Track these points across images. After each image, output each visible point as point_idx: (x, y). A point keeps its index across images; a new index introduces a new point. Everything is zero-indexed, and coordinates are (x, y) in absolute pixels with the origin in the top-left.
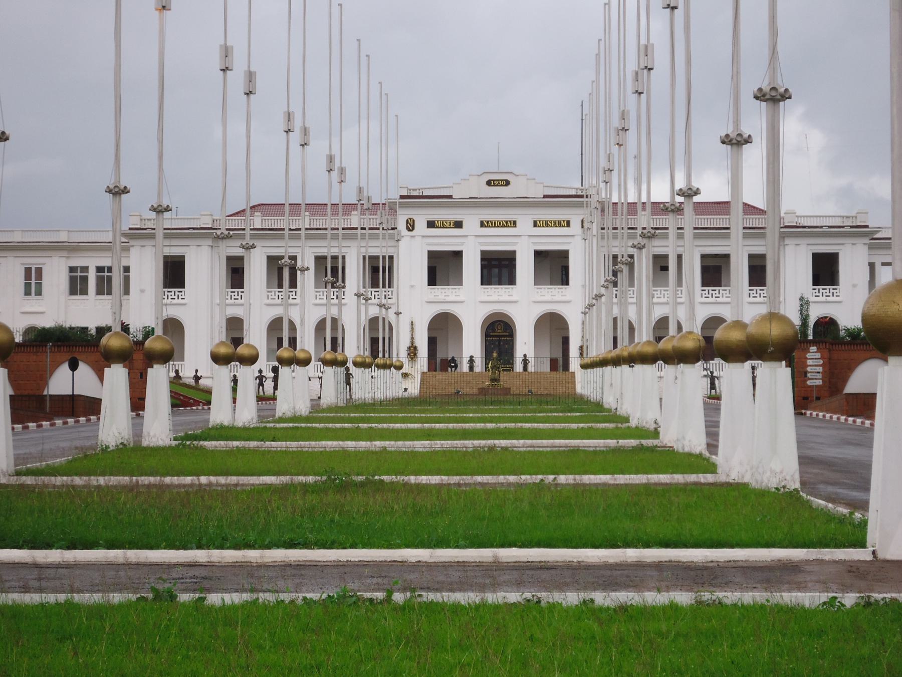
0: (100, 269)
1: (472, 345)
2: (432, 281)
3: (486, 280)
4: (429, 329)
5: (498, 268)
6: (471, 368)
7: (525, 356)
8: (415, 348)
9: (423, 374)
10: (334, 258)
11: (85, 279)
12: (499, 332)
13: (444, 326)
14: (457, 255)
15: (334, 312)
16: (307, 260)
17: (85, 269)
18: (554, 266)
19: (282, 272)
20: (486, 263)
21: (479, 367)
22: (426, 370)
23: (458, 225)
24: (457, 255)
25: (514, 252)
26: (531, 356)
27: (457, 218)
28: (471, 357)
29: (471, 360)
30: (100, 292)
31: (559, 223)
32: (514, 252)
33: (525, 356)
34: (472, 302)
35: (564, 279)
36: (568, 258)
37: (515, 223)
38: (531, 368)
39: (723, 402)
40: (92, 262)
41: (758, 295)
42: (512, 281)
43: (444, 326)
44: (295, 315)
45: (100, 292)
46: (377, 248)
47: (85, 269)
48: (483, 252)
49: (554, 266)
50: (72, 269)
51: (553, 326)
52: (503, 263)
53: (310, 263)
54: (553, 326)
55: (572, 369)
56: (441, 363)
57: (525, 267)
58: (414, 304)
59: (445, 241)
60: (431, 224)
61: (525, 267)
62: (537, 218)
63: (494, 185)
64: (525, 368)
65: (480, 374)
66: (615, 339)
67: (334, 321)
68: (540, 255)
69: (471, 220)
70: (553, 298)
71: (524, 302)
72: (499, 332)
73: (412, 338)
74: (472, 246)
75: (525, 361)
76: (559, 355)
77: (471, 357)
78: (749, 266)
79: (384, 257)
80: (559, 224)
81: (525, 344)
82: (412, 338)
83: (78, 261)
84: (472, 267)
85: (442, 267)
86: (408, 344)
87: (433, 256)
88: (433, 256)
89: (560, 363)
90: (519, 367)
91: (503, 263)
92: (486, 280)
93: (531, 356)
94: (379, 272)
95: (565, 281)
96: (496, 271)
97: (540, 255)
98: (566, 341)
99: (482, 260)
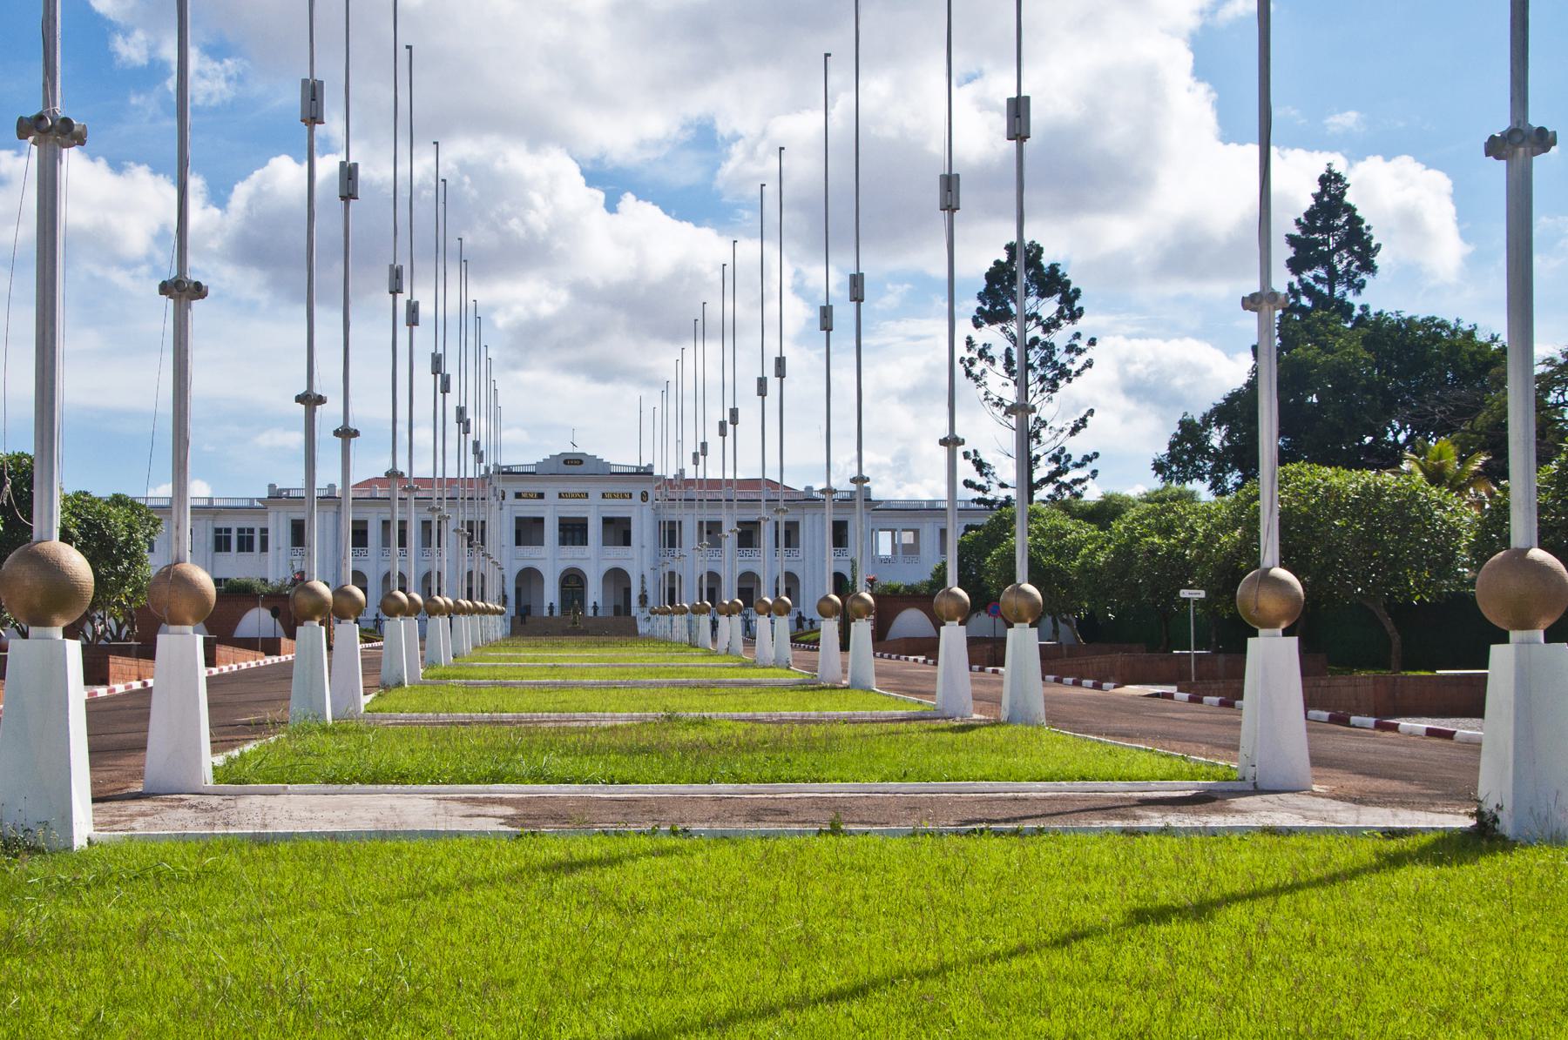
0: (240, 530)
1: (551, 594)
2: (518, 543)
3: (563, 541)
4: (517, 581)
5: (573, 531)
11: (228, 539)
12: (573, 582)
13: (529, 578)
14: (541, 520)
17: (228, 530)
18: (619, 531)
19: (748, 536)
21: (557, 613)
23: (541, 496)
24: (541, 520)
26: (557, 604)
30: (240, 549)
34: (551, 559)
35: (626, 541)
38: (600, 614)
40: (234, 524)
42: (541, 543)
43: (529, 578)
45: (240, 549)
46: (476, 515)
47: (228, 530)
49: (619, 531)
50: (218, 530)
51: (617, 578)
54: (617, 578)
57: (595, 530)
58: (504, 557)
59: (529, 509)
60: (518, 495)
61: (595, 530)
68: (607, 521)
69: (551, 491)
70: (616, 556)
71: (594, 559)
74: (551, 512)
75: (595, 608)
80: (623, 496)
81: (594, 593)
83: (222, 524)
84: (551, 531)
85: (528, 531)
87: (520, 521)
88: (520, 521)
89: (623, 609)
92: (563, 541)
93: (600, 604)
94: (475, 534)
96: (569, 535)
97: (607, 521)
98: (628, 591)
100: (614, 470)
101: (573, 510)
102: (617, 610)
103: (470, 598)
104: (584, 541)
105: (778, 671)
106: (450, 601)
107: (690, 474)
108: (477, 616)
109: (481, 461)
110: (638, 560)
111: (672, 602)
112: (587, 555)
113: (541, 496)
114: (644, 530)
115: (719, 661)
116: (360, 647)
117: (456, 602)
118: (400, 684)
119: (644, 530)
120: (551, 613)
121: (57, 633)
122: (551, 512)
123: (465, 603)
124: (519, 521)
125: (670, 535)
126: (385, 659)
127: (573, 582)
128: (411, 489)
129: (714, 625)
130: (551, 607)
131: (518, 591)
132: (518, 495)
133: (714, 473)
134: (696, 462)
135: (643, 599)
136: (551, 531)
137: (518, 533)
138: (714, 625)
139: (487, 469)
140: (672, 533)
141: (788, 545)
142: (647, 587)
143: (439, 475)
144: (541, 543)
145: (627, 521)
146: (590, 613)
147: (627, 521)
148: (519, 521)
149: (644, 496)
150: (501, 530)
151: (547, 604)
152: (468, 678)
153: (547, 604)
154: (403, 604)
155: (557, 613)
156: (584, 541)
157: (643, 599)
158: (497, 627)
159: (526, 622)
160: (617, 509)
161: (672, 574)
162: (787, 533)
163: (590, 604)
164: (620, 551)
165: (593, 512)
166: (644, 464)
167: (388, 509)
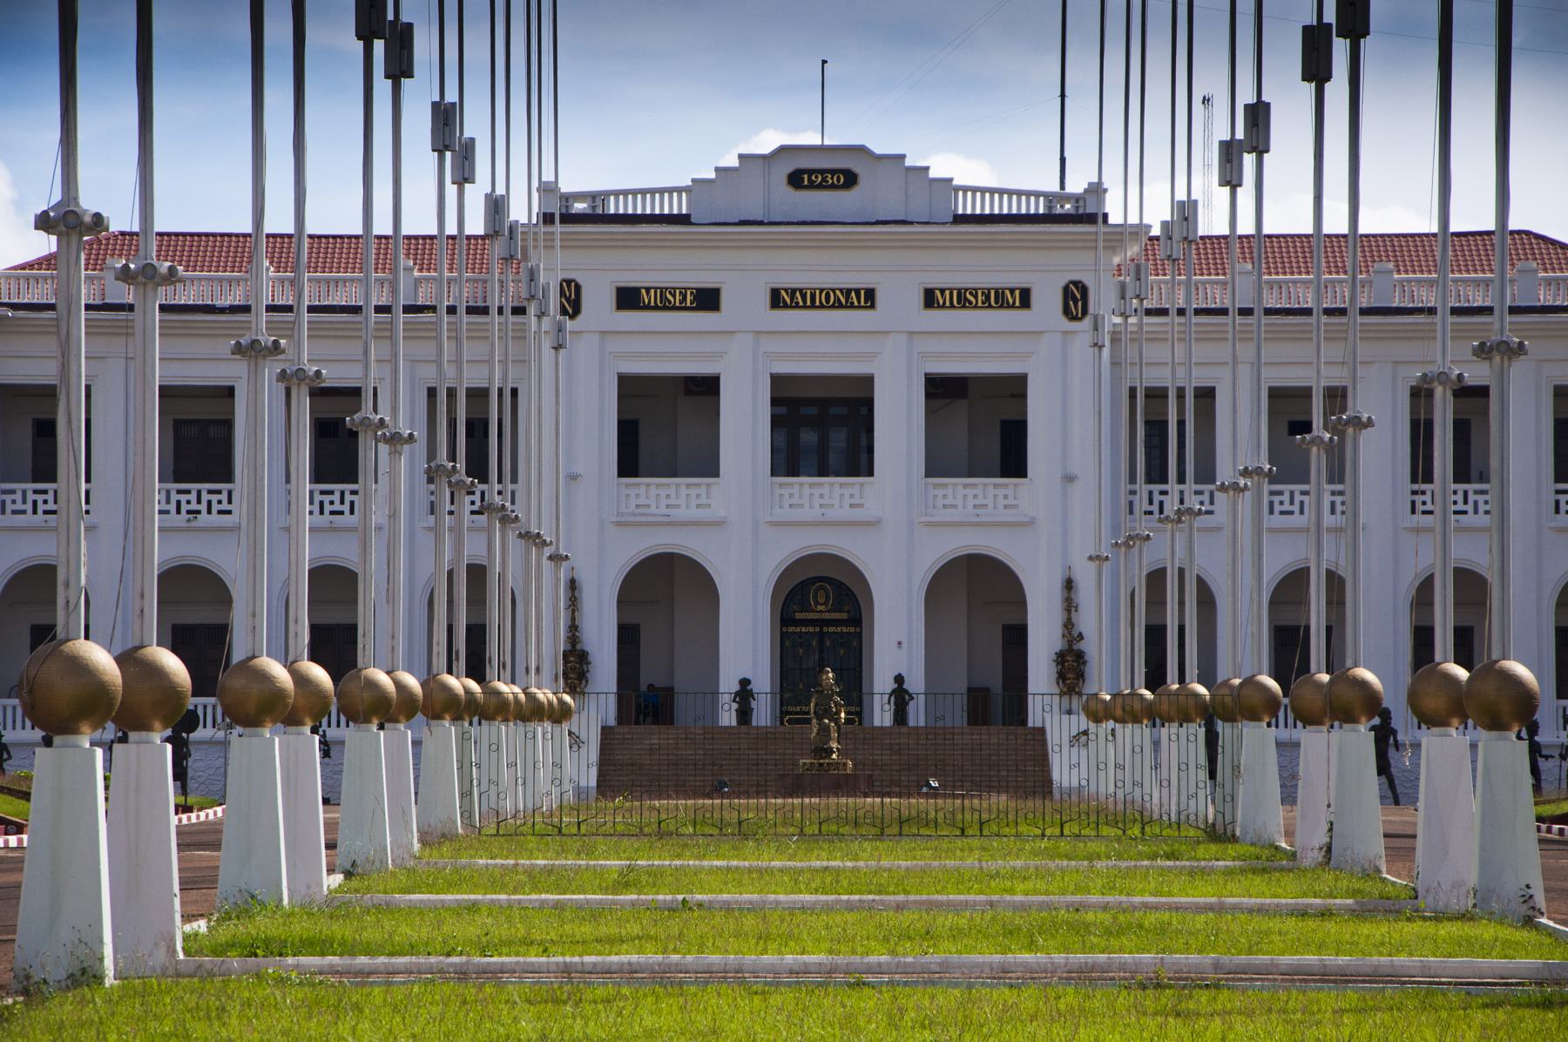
1: (745, 648)
2: (629, 466)
4: (621, 602)
6: (744, 714)
7: (899, 679)
8: (1080, 657)
9: (606, 731)
10: (478, 395)
12: (821, 610)
13: (666, 590)
14: (706, 388)
15: (1332, 555)
16: (397, 406)
18: (983, 425)
20: (783, 410)
21: (763, 713)
22: (612, 722)
23: (708, 300)
24: (706, 388)
25: (868, 381)
26: (763, 683)
27: (705, 280)
28: (745, 682)
29: (744, 693)
31: (1000, 294)
32: (868, 381)
33: (899, 679)
34: (744, 523)
35: (1011, 459)
36: (1024, 396)
37: (870, 294)
38: (917, 715)
39: (1420, 844)
41: (1470, 508)
42: (708, 466)
43: (666, 590)
44: (1209, 559)
48: (777, 380)
51: (977, 591)
52: (804, 411)
53: (406, 416)
54: (977, 591)
55: (1034, 720)
56: (645, 703)
57: (899, 424)
58: (583, 519)
59: (668, 344)
60: (628, 299)
61: (899, 424)
62: (936, 281)
63: (812, 186)
64: (900, 716)
65: (765, 735)
66: (1155, 636)
67: (1335, 583)
68: (943, 391)
69: (745, 279)
70: (976, 516)
71: (896, 525)
72: (821, 611)
73: (573, 628)
74: (744, 360)
75: (900, 695)
76: (994, 679)
77: (745, 682)
78: (620, 422)
79: (1181, 394)
80: (997, 299)
81: (897, 646)
82: (573, 628)
84: (744, 424)
85: (661, 425)
86: (1058, 644)
87: (637, 394)
89: (998, 702)
90: (882, 715)
91: (804, 411)
92: (789, 459)
93: (916, 683)
94: (477, 438)
95: (1013, 462)
96: (808, 437)
97: (943, 391)
98: (1016, 637)
99: (775, 402)
100: (966, 206)
101: (822, 348)
102: (979, 706)
103: (476, 670)
104: (859, 462)
105: (1486, 931)
106: (412, 682)
107: (1212, 222)
108: (449, 730)
109: (464, 177)
110: (1057, 525)
111: (1155, 679)
112: (718, 510)
113: (708, 300)
114: (1072, 423)
115: (1286, 892)
116: (174, 820)
117: (429, 682)
118: (85, 976)
119: (1072, 423)
120: (744, 714)
121: (374, 728)
122: (744, 360)
123: (458, 683)
124: (632, 389)
125: (1164, 438)
126: (32, 884)
127: (821, 610)
128: (146, 277)
129: (1288, 750)
130: (744, 693)
131: (628, 637)
132: (628, 299)
133: (1288, 215)
134: (1231, 180)
135: (1071, 666)
136: (744, 424)
137: (628, 434)
138: (1288, 750)
139: (496, 206)
140: (477, 429)
141: (1463, 471)
142: (1087, 622)
143: (451, 229)
144: (708, 466)
145: (1014, 388)
146: (882, 715)
147: (1014, 388)
148: (632, 389)
149: (1075, 300)
150: (567, 422)
151: (728, 684)
152: (350, 949)
153: (728, 684)
154: (278, 694)
155: (763, 713)
156: (859, 462)
157: (1071, 666)
158: (553, 763)
159: (659, 736)
160: (976, 343)
161: (477, 574)
162: (1462, 431)
163: (882, 683)
164: (989, 492)
165: (893, 356)
166: (1076, 186)
167: (50, 345)
